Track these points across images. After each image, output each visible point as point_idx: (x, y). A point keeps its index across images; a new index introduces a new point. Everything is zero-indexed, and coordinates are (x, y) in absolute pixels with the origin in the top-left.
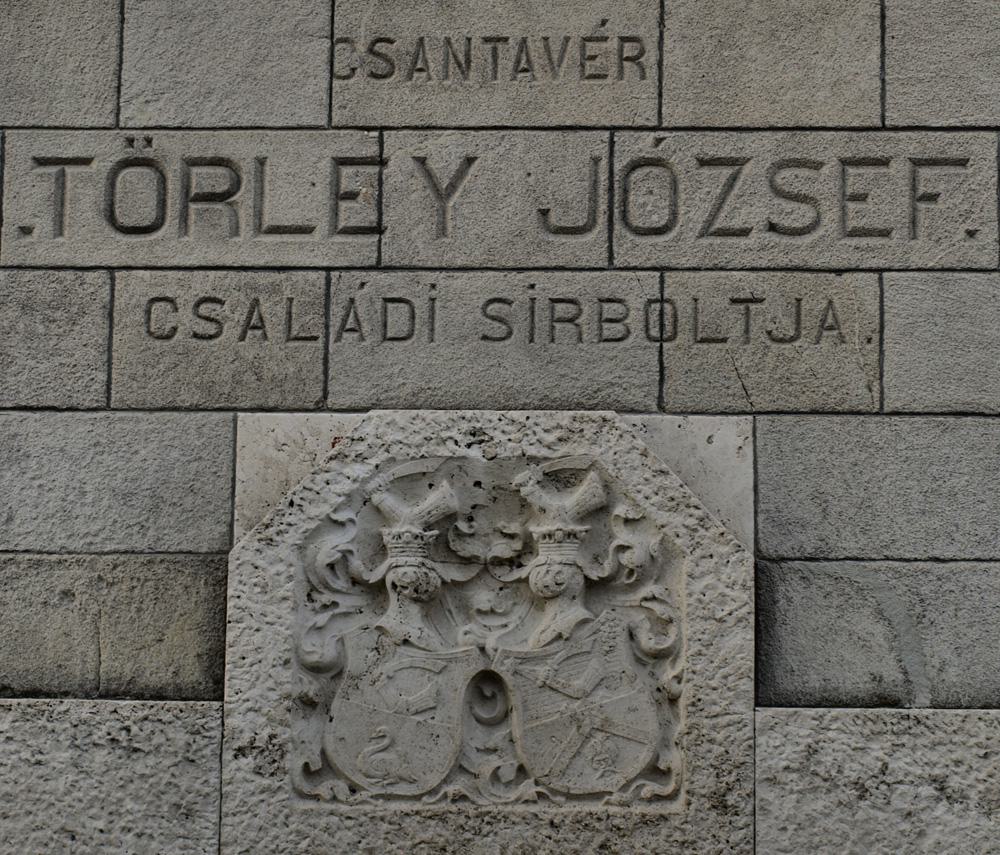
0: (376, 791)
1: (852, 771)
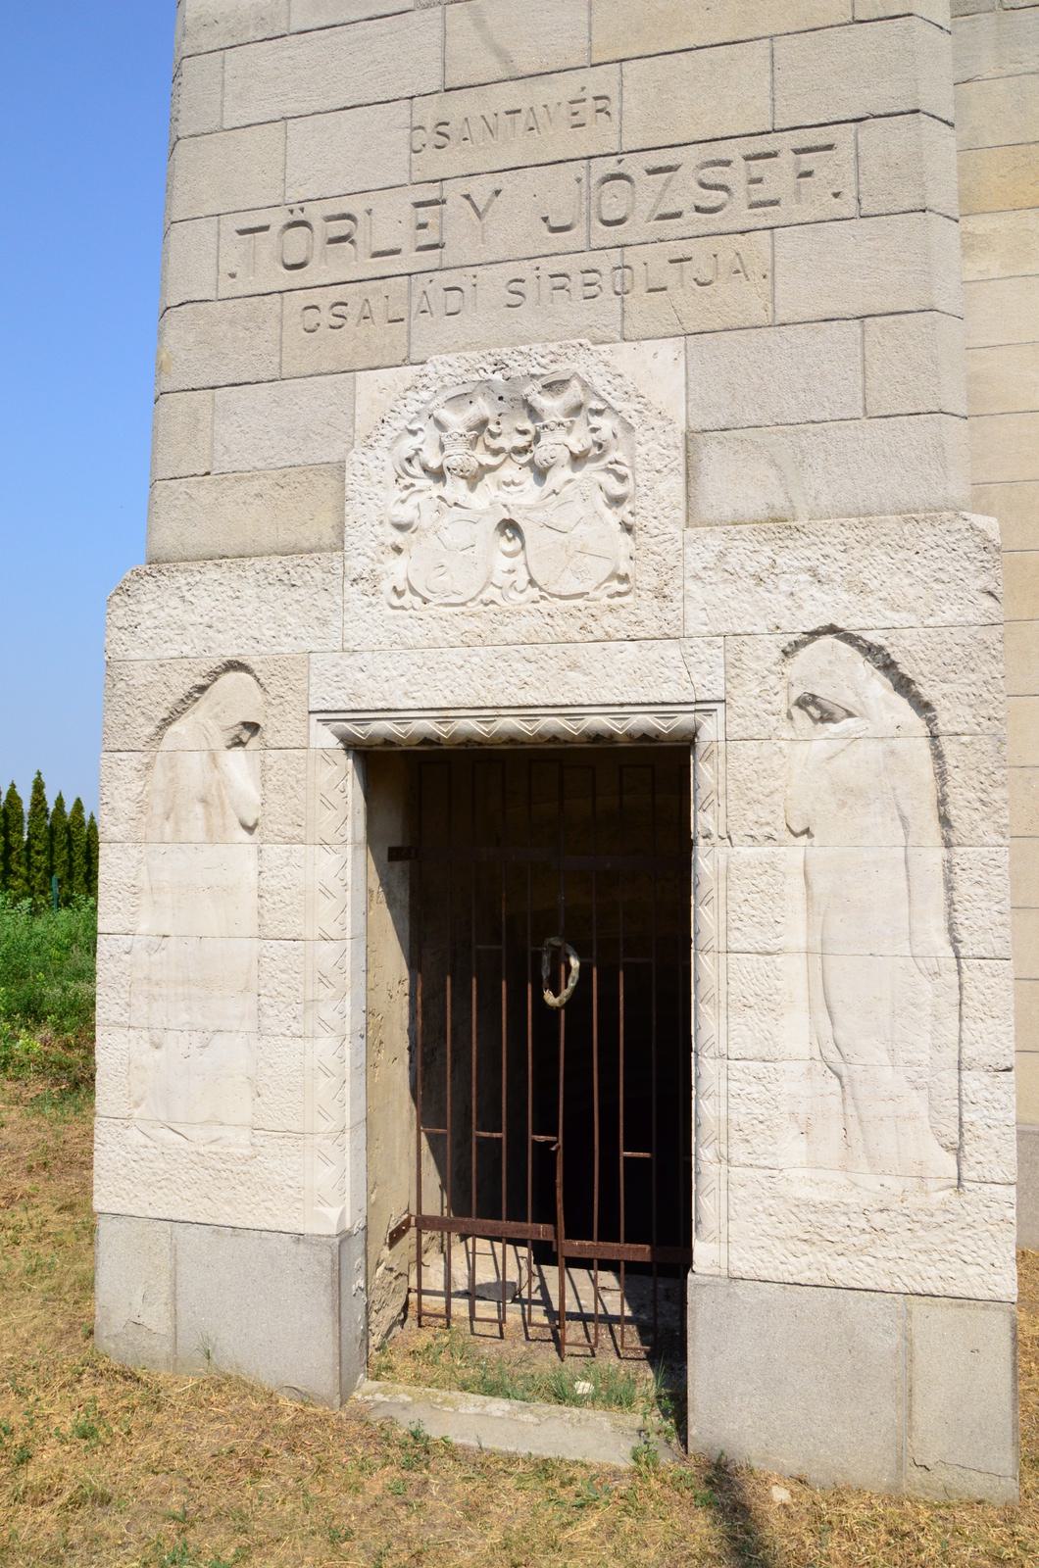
0: (438, 601)
1: (752, 567)
